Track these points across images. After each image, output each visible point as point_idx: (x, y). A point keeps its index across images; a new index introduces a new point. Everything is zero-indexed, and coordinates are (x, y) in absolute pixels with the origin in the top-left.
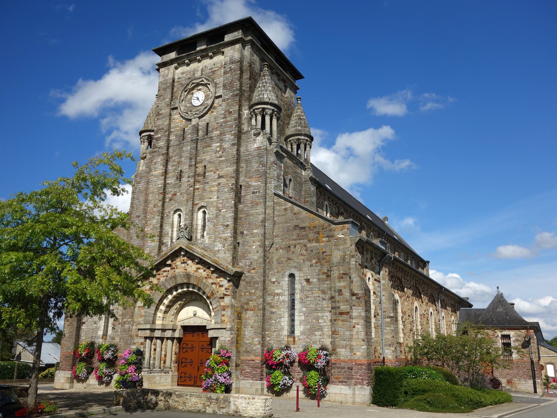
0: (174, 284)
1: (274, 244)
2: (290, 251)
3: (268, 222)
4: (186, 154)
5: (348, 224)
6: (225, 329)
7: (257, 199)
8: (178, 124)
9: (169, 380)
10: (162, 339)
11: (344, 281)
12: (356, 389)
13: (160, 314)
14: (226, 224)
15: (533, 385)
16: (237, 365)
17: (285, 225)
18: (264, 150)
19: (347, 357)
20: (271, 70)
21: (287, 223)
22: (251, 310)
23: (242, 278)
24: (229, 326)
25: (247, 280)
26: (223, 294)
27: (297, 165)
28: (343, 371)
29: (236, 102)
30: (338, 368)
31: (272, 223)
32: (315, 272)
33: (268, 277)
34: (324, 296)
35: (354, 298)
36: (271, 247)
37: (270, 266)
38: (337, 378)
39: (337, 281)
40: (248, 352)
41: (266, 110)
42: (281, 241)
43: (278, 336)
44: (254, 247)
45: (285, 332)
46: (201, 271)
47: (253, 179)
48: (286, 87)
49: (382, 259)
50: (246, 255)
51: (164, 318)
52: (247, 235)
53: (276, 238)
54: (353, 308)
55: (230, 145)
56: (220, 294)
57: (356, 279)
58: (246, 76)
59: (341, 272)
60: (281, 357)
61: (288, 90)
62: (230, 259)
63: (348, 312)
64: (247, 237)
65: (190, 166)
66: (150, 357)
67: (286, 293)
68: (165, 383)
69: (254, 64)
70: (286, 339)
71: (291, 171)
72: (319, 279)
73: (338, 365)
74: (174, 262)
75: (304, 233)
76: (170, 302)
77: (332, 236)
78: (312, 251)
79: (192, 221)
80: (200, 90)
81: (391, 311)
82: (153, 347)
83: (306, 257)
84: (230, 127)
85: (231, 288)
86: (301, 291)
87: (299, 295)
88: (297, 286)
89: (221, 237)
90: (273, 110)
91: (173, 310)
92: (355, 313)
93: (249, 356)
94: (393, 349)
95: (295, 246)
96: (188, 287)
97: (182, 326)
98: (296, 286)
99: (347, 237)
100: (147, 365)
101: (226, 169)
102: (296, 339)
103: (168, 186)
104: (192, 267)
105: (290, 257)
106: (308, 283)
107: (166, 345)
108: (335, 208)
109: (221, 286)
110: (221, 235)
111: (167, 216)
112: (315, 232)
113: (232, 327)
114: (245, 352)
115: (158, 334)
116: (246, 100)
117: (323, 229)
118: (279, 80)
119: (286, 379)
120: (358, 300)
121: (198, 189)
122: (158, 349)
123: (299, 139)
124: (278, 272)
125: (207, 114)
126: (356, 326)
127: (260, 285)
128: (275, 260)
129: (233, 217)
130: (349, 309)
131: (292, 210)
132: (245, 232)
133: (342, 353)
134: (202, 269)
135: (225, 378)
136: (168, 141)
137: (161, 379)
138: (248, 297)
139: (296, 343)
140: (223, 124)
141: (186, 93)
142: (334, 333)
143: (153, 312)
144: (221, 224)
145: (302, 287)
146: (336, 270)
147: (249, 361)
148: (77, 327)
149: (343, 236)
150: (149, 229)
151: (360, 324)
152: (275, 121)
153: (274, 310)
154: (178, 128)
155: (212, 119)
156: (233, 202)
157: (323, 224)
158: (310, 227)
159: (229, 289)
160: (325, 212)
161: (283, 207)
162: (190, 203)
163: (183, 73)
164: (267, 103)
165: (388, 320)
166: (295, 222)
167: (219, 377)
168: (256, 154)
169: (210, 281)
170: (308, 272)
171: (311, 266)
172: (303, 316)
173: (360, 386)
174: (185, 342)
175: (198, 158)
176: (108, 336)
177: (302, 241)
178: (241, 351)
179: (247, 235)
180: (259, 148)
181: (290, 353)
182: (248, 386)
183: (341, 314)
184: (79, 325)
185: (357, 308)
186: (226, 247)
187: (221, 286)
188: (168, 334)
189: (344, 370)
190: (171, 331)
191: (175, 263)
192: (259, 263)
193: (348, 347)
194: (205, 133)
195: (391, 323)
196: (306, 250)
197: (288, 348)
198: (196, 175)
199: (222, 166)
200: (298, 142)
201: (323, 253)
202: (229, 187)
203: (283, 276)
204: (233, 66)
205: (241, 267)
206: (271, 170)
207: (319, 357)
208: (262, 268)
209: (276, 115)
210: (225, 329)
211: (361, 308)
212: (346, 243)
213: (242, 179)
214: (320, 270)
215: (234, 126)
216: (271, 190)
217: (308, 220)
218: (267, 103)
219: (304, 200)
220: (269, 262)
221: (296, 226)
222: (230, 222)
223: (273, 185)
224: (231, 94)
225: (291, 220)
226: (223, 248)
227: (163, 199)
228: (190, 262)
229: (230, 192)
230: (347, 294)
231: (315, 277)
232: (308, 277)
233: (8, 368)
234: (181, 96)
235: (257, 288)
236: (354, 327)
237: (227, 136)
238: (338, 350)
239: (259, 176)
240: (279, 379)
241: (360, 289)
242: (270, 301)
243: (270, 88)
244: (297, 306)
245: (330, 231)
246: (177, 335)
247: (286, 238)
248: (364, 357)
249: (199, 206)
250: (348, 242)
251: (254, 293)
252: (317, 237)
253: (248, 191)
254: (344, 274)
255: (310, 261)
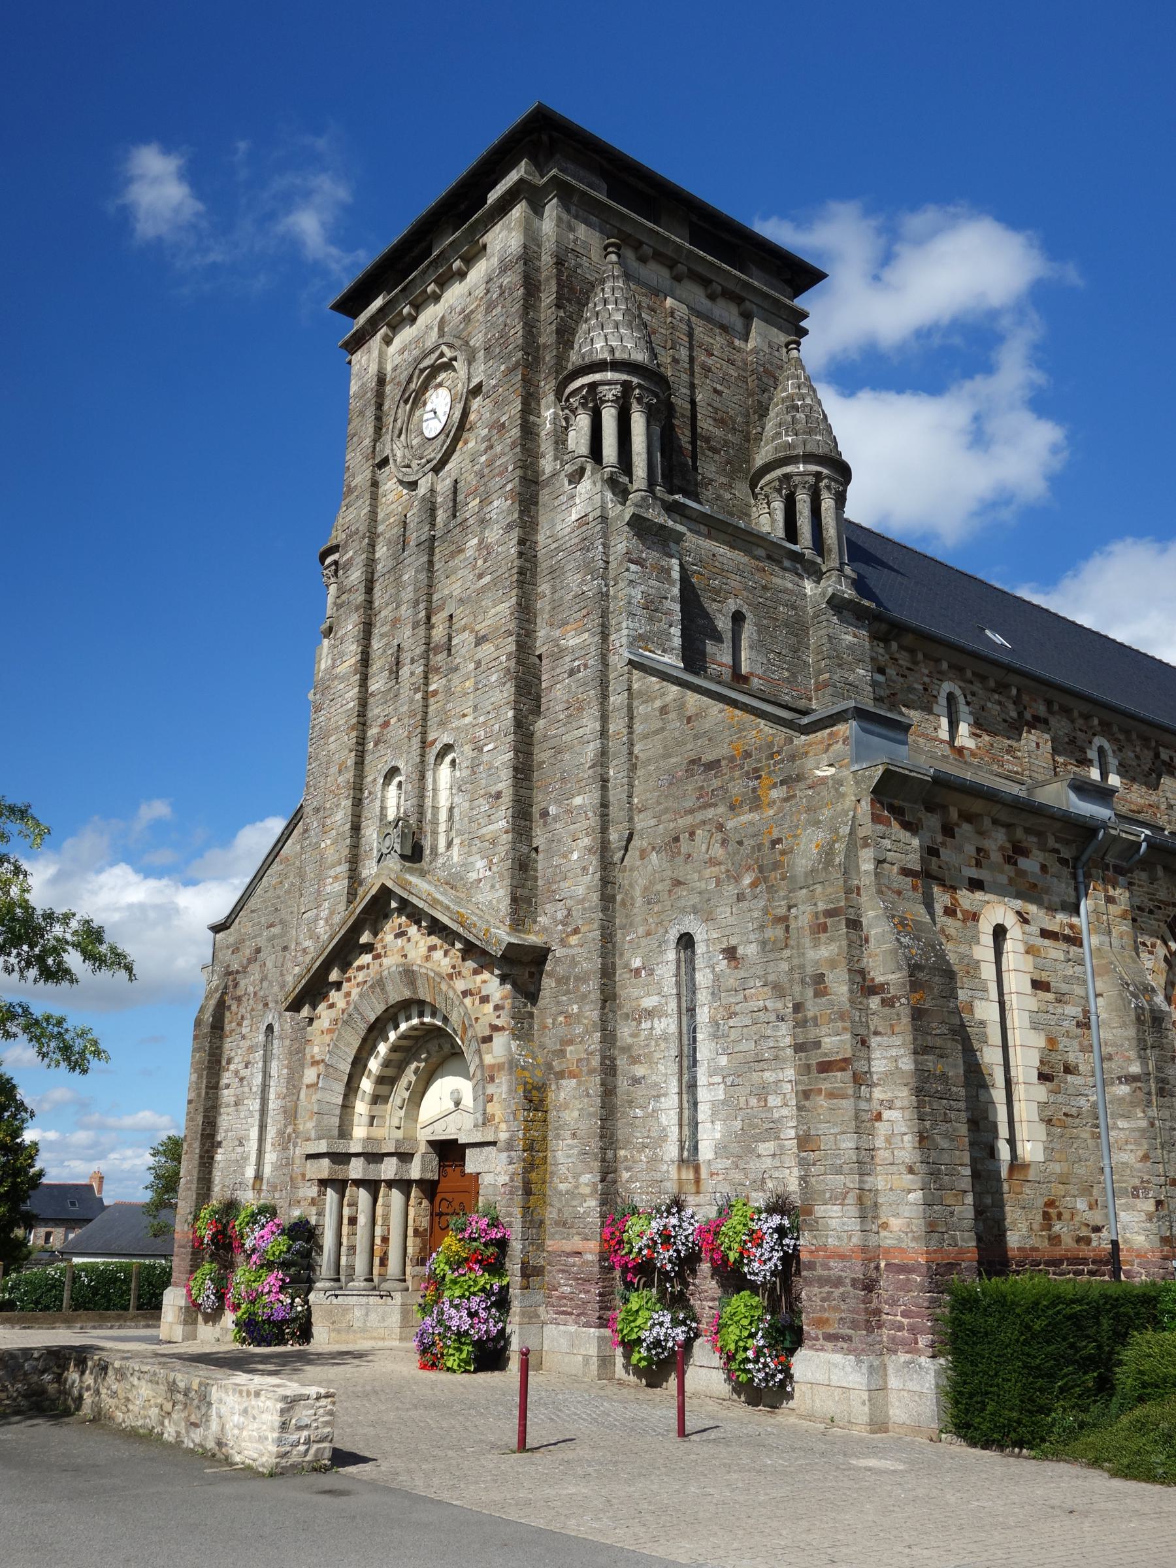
0: (384, 1007)
1: (636, 837)
2: (679, 853)
3: (615, 762)
4: (408, 594)
5: (846, 721)
6: (494, 1143)
7: (581, 690)
8: (393, 506)
9: (395, 1318)
10: (373, 1186)
11: (831, 940)
12: (890, 1371)
13: (361, 1107)
14: (493, 790)
15: (529, 1406)
16: (529, 1272)
17: (662, 764)
18: (594, 523)
19: (850, 1237)
20: (671, 268)
21: (669, 756)
22: (572, 1075)
23: (547, 968)
24: (503, 1136)
25: (560, 970)
26: (490, 1025)
27: (778, 562)
28: (837, 1292)
29: (515, 387)
30: (823, 1281)
31: (626, 766)
32: (752, 920)
33: (622, 955)
34: (779, 1005)
35: (874, 1002)
36: (626, 850)
37: (627, 916)
38: (820, 1323)
39: (807, 942)
40: (564, 1224)
41: (600, 388)
42: (653, 822)
43: (654, 1161)
44: (575, 856)
45: (671, 1151)
46: (438, 955)
47: (569, 627)
48: (747, 317)
49: (1082, 853)
50: (554, 887)
51: (373, 1118)
52: (556, 818)
53: (641, 816)
54: (874, 1041)
55: (501, 532)
56: (482, 1030)
57: (879, 930)
58: (547, 297)
59: (822, 906)
60: (644, 1241)
61: (756, 322)
62: (504, 906)
63: (845, 1060)
64: (557, 826)
65: (415, 626)
66: (340, 1244)
67: (672, 1005)
68: (381, 1331)
69: (578, 255)
70: (673, 1170)
71: (740, 586)
72: (763, 943)
73: (820, 1271)
74: (379, 937)
75: (716, 783)
76: (386, 1064)
77: (800, 778)
78: (740, 843)
79: (422, 796)
80: (440, 385)
81: (1132, 1054)
82: (346, 1212)
83: (723, 868)
84: (501, 474)
85: (508, 1003)
86: (713, 993)
87: (706, 1009)
88: (703, 978)
89: (483, 835)
90: (626, 385)
91: (400, 1093)
92: (879, 1066)
93: (567, 1237)
94: (1150, 1206)
95: (692, 834)
96: (421, 1015)
97: (432, 1143)
98: (698, 976)
99: (846, 773)
100: (329, 1268)
101: (493, 611)
102: (704, 1173)
103: (371, 700)
104: (418, 943)
105: (680, 874)
106: (733, 964)
107: (387, 1206)
108: (1000, 703)
109: (485, 999)
110: (484, 831)
111: (370, 793)
112: (747, 773)
113: (511, 1139)
114: (557, 1223)
115: (356, 1170)
116: (549, 374)
117: (771, 756)
118: (712, 297)
119: (661, 1324)
120: (886, 1011)
121: (435, 693)
122: (362, 1220)
123: (787, 477)
124: (648, 934)
125: (454, 451)
126: (887, 1114)
127: (592, 987)
128: (638, 892)
129: (510, 764)
130: (848, 1046)
131: (682, 706)
132: (552, 810)
133: (833, 1223)
134: (441, 947)
135: (471, 1315)
136: (371, 563)
137: (367, 1315)
138: (562, 1031)
139: (702, 1188)
140: (486, 471)
141: (408, 407)
142: (805, 1142)
143: (340, 1101)
144: (482, 792)
145: (717, 978)
146: (804, 903)
147: (569, 1255)
148: (201, 1157)
149: (832, 770)
150: (328, 842)
151: (898, 1103)
152: (638, 423)
153: (640, 1071)
154: (392, 520)
155: (467, 464)
156: (511, 714)
157: (770, 739)
158: (732, 759)
159: (503, 1008)
160: (944, 722)
161: (658, 704)
162: (416, 742)
163: (401, 352)
164: (600, 366)
165: (1123, 1090)
166: (691, 749)
167: (453, 1311)
168: (577, 540)
169: (460, 985)
170: (732, 920)
171: (740, 897)
172: (722, 1086)
173: (903, 1357)
174: (443, 1196)
175: (435, 597)
176: (265, 1181)
177: (710, 813)
178: (548, 1222)
179: (556, 818)
180: (583, 520)
181: (674, 1227)
182: (564, 1343)
183: (825, 1067)
184: (207, 1151)
185: (884, 1040)
186: (494, 868)
187: (485, 999)
188: (389, 1169)
189: (841, 1290)
190: (394, 1160)
191: (382, 940)
192: (590, 908)
193: (851, 1199)
194: (449, 513)
195: (1133, 1104)
196: (724, 843)
197: (678, 1205)
198: (429, 648)
199: (483, 603)
200: (789, 488)
201: (774, 842)
202: (500, 667)
203: (662, 944)
204: (505, 280)
205: (545, 929)
206: (622, 585)
207: (756, 1238)
208: (596, 926)
209: (639, 400)
210: (494, 1143)
211: (897, 1040)
212: (843, 795)
213: (542, 631)
214: (765, 911)
215: (510, 468)
216: (620, 655)
217: (727, 733)
218: (600, 366)
219: (816, 682)
220: (623, 902)
221: (693, 762)
222: (504, 784)
223: (625, 632)
224: (503, 368)
225: (678, 744)
226: (488, 873)
227: (358, 743)
228: (413, 930)
229: (505, 683)
230: (840, 987)
231: (752, 937)
232: (733, 941)
233: (119, 1279)
234: (395, 420)
235: (584, 997)
236: (879, 1117)
237: (496, 504)
238: (819, 1210)
239: (584, 612)
240: (639, 1321)
241: (893, 966)
242: (630, 1040)
243: (618, 317)
244: (704, 1051)
245: (792, 758)
246: (415, 1171)
247: (666, 811)
248: (914, 1239)
249: (438, 746)
250: (849, 789)
251: (578, 1015)
252: (754, 790)
253: (558, 671)
254: (829, 913)
255: (737, 879)
